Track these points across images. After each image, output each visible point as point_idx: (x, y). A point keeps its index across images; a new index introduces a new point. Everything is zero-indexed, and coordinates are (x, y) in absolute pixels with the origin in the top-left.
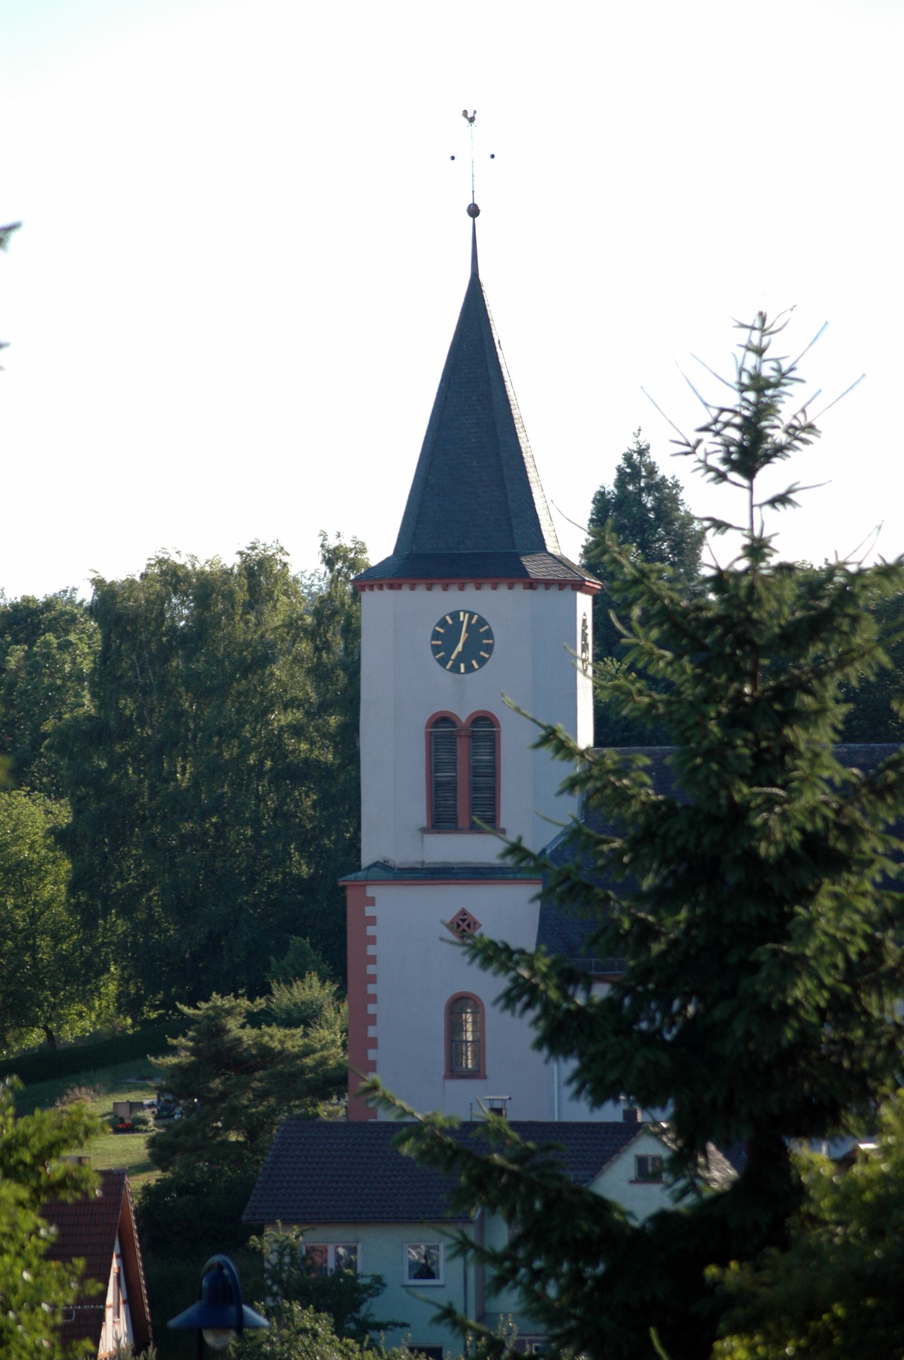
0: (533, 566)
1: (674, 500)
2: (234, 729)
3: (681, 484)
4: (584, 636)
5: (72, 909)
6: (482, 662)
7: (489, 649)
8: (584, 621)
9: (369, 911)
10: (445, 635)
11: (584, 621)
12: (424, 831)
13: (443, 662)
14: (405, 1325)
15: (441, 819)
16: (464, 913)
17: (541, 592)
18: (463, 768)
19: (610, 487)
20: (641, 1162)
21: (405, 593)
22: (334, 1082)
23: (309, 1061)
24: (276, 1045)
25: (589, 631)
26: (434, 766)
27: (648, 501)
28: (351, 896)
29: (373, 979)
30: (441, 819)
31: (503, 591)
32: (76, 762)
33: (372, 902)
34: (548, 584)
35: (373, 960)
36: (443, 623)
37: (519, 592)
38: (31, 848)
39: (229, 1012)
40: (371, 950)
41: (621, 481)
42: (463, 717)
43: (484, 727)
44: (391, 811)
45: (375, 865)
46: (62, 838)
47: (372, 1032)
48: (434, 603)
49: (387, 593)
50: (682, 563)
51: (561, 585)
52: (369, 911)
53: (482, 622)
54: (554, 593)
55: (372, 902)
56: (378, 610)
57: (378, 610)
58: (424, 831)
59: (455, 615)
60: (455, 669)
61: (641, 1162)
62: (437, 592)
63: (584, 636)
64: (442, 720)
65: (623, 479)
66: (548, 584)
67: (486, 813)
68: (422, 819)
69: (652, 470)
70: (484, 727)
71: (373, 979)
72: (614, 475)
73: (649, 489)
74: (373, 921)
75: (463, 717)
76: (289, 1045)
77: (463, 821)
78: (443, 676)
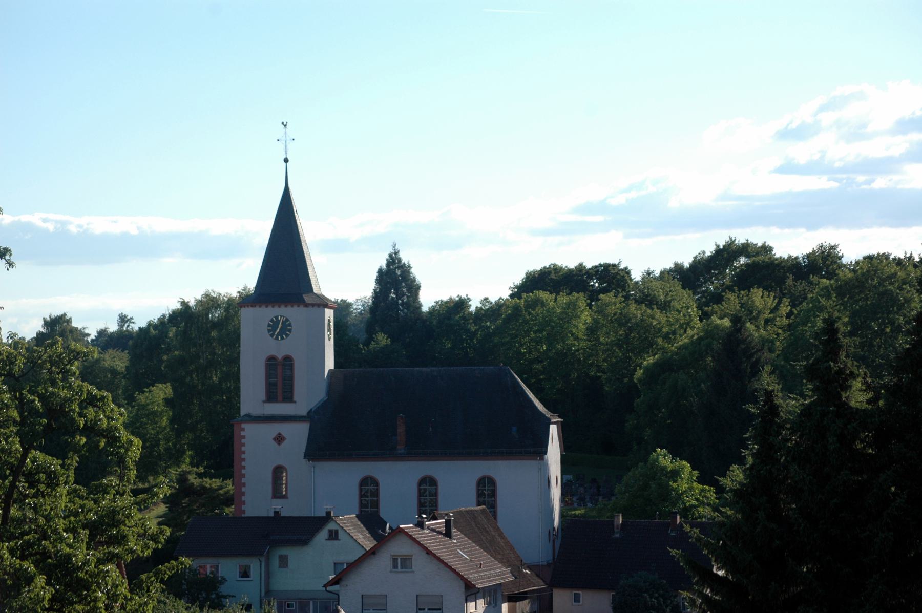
0: (307, 298)
1: (409, 273)
2: (780, 331)
3: (651, 270)
4: (329, 325)
5: (172, 429)
6: (287, 336)
7: (290, 331)
8: (329, 321)
9: (242, 433)
10: (273, 325)
11: (329, 321)
12: (264, 402)
13: (272, 336)
14: (233, 596)
15: (271, 397)
16: (280, 434)
17: (310, 308)
18: (280, 378)
19: (384, 267)
20: (330, 531)
21: (257, 309)
22: (229, 500)
23: (221, 492)
24: (208, 486)
25: (332, 324)
26: (268, 376)
27: (398, 272)
28: (236, 428)
29: (244, 460)
30: (271, 397)
31: (295, 308)
32: (15, 382)
33: (243, 430)
34: (313, 305)
35: (244, 452)
36: (272, 320)
37: (302, 308)
38: (158, 405)
39: (189, 473)
40: (243, 448)
41: (388, 264)
42: (280, 357)
43: (288, 361)
44: (252, 394)
45: (246, 415)
46: (168, 402)
47: (243, 480)
48: (268, 313)
49: (251, 309)
50: (411, 296)
51: (319, 305)
52: (242, 433)
53: (287, 320)
54: (316, 309)
55: (243, 430)
56: (246, 314)
57: (246, 314)
58: (264, 402)
59: (276, 317)
60: (277, 338)
61: (330, 531)
62: (270, 308)
63: (329, 325)
64: (271, 359)
65: (389, 264)
66: (313, 305)
67: (288, 397)
68: (264, 398)
69: (400, 260)
70: (288, 361)
71: (244, 460)
72: (386, 262)
73: (399, 268)
74: (244, 437)
75: (280, 357)
76: (213, 486)
77: (280, 398)
78: (272, 341)
